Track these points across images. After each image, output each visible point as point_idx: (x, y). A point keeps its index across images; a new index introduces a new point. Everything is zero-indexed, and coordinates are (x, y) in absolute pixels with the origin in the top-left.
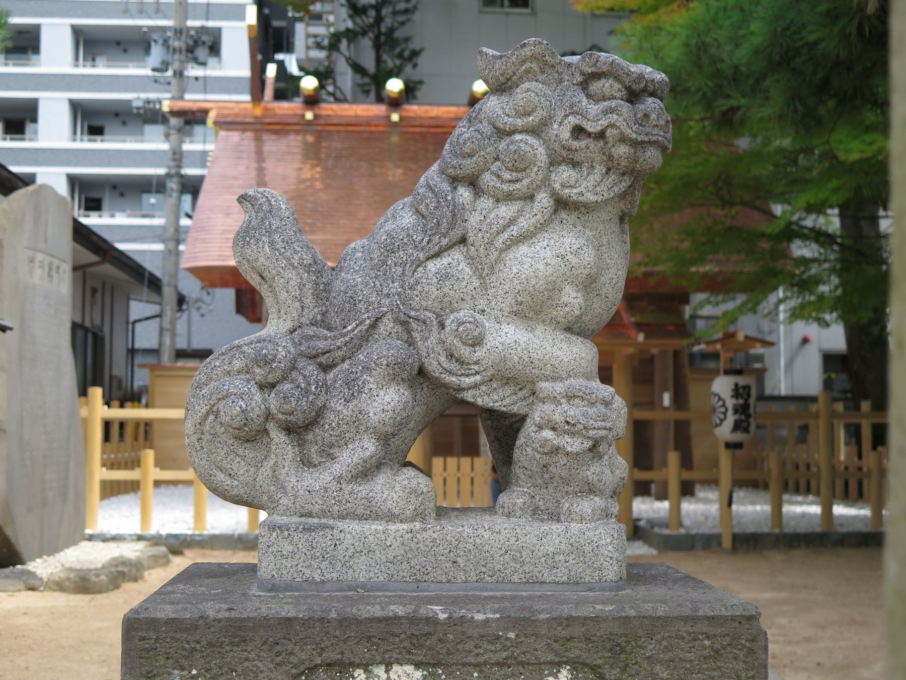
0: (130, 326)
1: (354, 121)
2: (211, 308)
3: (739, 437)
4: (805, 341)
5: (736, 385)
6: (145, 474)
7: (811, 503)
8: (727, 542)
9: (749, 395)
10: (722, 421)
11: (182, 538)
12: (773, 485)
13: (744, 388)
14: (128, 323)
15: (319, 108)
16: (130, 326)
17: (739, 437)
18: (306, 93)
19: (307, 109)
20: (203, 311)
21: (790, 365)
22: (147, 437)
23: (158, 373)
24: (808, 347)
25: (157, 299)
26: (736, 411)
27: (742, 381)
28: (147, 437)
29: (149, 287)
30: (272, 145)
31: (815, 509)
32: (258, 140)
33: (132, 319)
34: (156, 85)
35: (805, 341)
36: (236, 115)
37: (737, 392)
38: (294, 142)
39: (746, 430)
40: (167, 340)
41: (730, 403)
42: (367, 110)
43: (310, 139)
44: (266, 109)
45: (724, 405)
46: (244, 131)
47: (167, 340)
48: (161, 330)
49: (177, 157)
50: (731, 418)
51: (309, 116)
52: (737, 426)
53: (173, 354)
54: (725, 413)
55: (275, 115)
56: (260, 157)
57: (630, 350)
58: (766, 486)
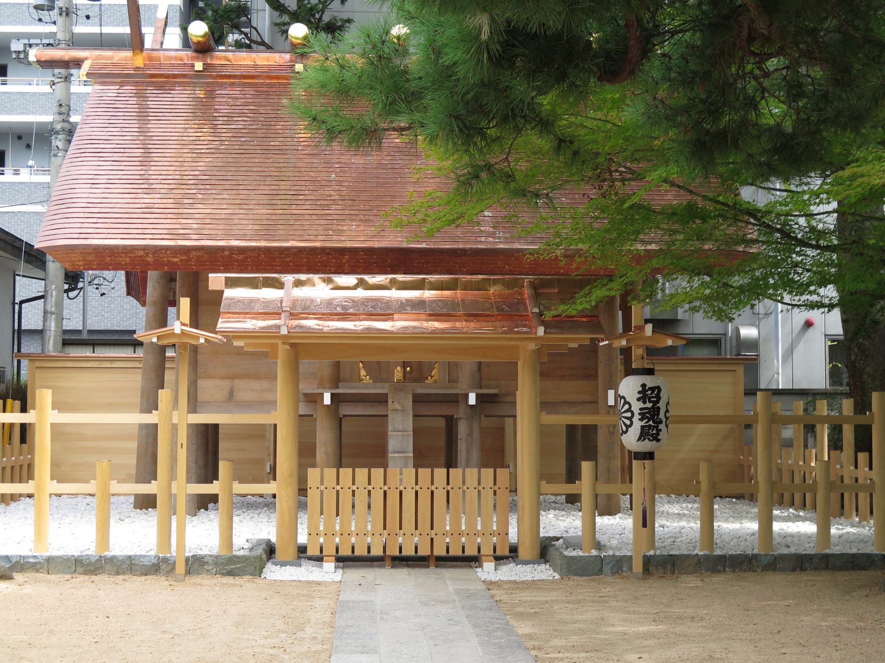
0: (17, 307)
1: (253, 72)
2: (112, 285)
3: (647, 446)
4: (808, 324)
5: (644, 386)
6: (39, 487)
7: (804, 519)
8: (638, 566)
9: (658, 398)
10: (628, 427)
11: (14, 561)
12: (762, 495)
13: (652, 389)
14: (14, 303)
15: (212, 57)
16: (17, 307)
17: (647, 446)
18: (195, 39)
19: (197, 59)
20: (103, 289)
21: (789, 353)
22: (23, 440)
23: (37, 364)
24: (811, 330)
25: (41, 274)
26: (643, 417)
27: (650, 381)
28: (23, 440)
29: (26, 261)
30: (157, 100)
31: (809, 528)
32: (140, 95)
33: (17, 301)
34: (40, 23)
35: (808, 324)
36: (115, 65)
37: (645, 394)
38: (181, 98)
39: (656, 438)
40: (52, 325)
41: (636, 406)
42: (268, 59)
43: (201, 94)
44: (150, 58)
45: (629, 410)
46: (122, 84)
47: (52, 325)
48: (45, 312)
49: (63, 110)
50: (637, 424)
51: (199, 66)
52: (644, 434)
53: (61, 342)
54: (630, 419)
55: (160, 66)
56: (143, 115)
57: (532, 346)
58: (752, 498)
